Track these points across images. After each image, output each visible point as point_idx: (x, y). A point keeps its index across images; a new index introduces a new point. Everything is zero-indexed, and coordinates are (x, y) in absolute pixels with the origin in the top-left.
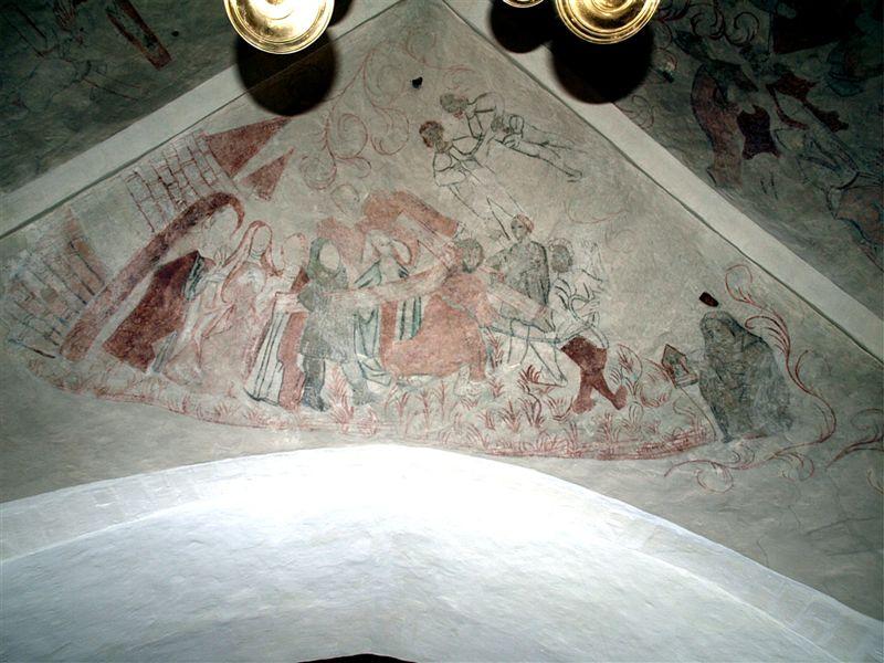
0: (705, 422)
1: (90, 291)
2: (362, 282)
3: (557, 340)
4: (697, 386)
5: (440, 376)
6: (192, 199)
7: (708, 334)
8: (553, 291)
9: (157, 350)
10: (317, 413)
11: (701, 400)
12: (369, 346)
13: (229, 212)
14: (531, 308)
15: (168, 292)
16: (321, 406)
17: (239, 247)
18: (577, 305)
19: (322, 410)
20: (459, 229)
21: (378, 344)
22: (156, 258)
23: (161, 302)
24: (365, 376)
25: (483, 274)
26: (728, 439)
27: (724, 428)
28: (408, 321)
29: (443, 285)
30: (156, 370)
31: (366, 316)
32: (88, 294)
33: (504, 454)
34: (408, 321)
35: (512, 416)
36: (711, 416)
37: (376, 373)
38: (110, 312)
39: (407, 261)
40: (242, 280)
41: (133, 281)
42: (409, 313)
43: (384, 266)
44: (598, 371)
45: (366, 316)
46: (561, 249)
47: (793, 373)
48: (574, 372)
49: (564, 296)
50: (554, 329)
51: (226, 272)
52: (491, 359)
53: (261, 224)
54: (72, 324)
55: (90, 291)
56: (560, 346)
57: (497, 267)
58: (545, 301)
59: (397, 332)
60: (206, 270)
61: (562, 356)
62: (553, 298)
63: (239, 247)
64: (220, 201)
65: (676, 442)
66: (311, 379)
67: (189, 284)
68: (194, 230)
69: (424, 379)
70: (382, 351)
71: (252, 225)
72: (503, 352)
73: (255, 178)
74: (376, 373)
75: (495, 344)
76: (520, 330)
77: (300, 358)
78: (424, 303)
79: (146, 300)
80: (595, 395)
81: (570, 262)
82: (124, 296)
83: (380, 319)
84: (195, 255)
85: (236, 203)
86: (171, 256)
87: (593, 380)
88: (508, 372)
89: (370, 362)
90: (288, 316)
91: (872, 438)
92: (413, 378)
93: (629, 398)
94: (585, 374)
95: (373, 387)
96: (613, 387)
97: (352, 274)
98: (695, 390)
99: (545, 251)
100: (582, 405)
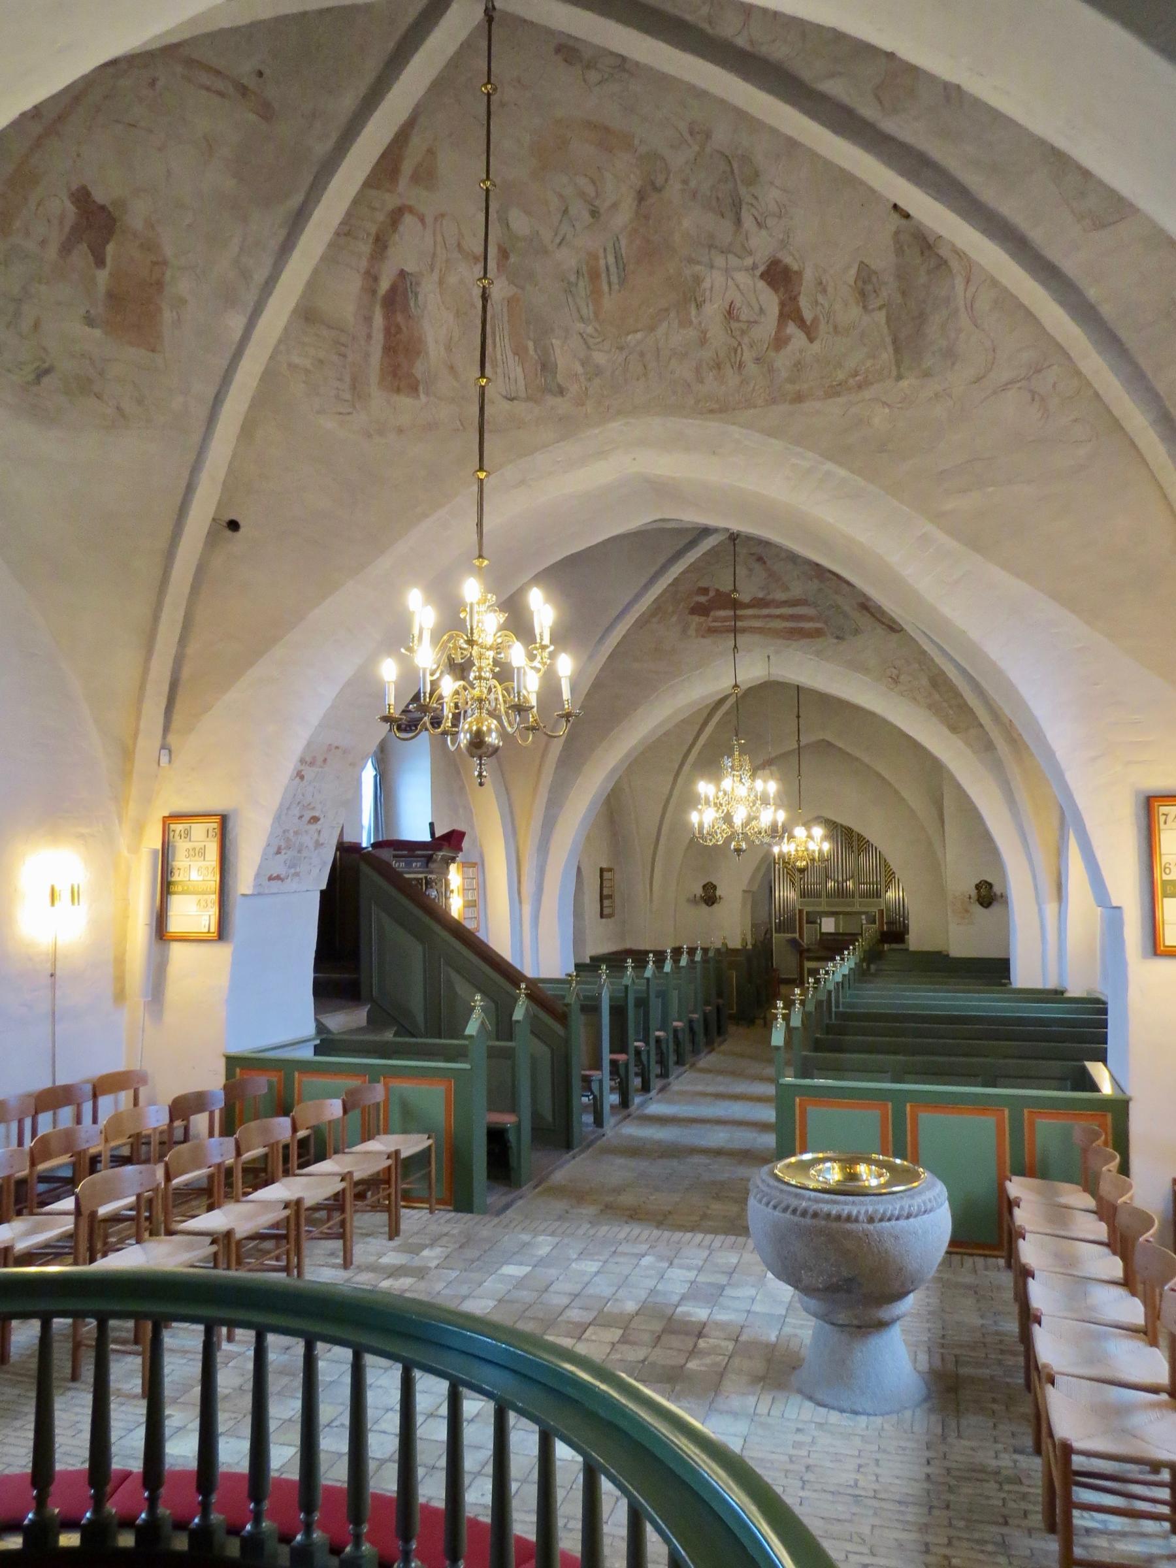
0: (885, 356)
1: (343, 345)
2: (558, 241)
3: (754, 267)
4: (883, 313)
5: (652, 329)
6: (373, 229)
7: (900, 251)
8: (744, 207)
9: (419, 376)
10: (559, 400)
11: (885, 331)
12: (584, 311)
13: (408, 219)
14: (724, 230)
15: (399, 318)
16: (561, 391)
17: (435, 246)
18: (770, 222)
19: (563, 396)
20: (636, 142)
21: (591, 307)
22: (374, 292)
23: (399, 329)
24: (589, 348)
25: (674, 191)
26: (899, 377)
27: (898, 364)
28: (613, 269)
29: (637, 213)
30: (427, 394)
31: (573, 278)
32: (343, 348)
33: (712, 411)
34: (613, 269)
35: (718, 366)
36: (890, 349)
37: (598, 340)
38: (367, 355)
39: (593, 194)
40: (452, 280)
41: (368, 320)
42: (611, 259)
43: (573, 211)
44: (794, 299)
45: (573, 278)
46: (746, 159)
47: (969, 305)
48: (770, 301)
49: (756, 213)
50: (750, 253)
51: (435, 276)
52: (695, 299)
53: (443, 215)
54: (347, 379)
55: (343, 345)
56: (758, 273)
57: (685, 182)
58: (738, 222)
59: (605, 288)
60: (418, 284)
61: (761, 284)
62: (748, 223)
63: (435, 246)
64: (396, 217)
65: (857, 378)
66: (546, 366)
67: (412, 304)
68: (391, 251)
69: (639, 336)
70: (596, 314)
71: (436, 219)
72: (705, 290)
73: (416, 178)
74: (598, 340)
75: (698, 280)
76: (720, 261)
77: (531, 344)
78: (624, 242)
79: (387, 331)
80: (791, 328)
81: (757, 174)
82: (369, 337)
83: (586, 275)
84: (402, 274)
85: (411, 210)
86: (384, 285)
87: (790, 312)
88: (713, 310)
89: (590, 330)
90: (506, 303)
91: (1022, 376)
92: (629, 337)
93: (823, 327)
94: (782, 304)
95: (600, 358)
96: (808, 315)
97: (546, 235)
98: (881, 317)
99: (730, 162)
100: (780, 342)
